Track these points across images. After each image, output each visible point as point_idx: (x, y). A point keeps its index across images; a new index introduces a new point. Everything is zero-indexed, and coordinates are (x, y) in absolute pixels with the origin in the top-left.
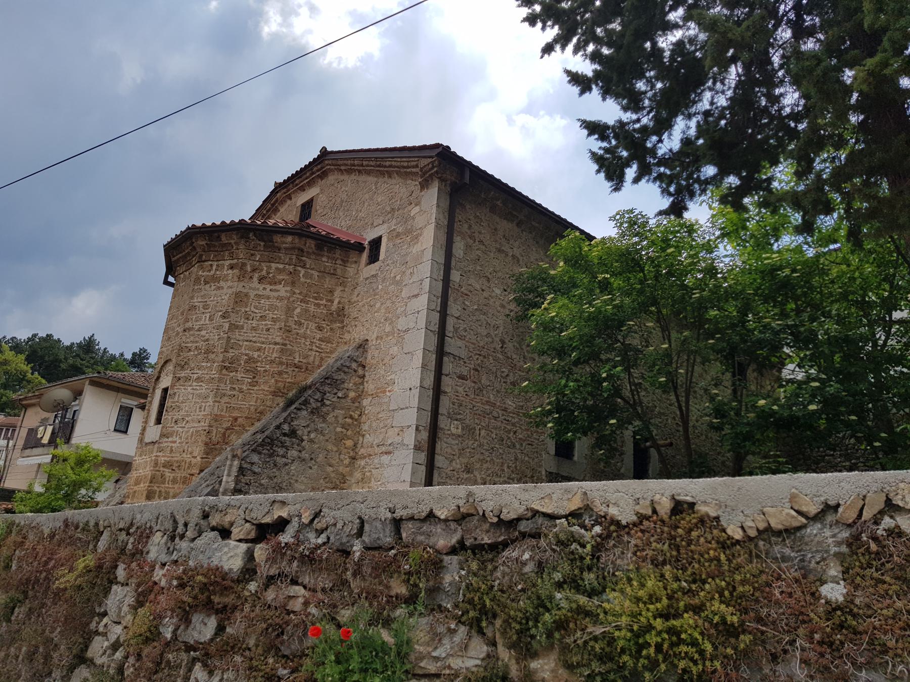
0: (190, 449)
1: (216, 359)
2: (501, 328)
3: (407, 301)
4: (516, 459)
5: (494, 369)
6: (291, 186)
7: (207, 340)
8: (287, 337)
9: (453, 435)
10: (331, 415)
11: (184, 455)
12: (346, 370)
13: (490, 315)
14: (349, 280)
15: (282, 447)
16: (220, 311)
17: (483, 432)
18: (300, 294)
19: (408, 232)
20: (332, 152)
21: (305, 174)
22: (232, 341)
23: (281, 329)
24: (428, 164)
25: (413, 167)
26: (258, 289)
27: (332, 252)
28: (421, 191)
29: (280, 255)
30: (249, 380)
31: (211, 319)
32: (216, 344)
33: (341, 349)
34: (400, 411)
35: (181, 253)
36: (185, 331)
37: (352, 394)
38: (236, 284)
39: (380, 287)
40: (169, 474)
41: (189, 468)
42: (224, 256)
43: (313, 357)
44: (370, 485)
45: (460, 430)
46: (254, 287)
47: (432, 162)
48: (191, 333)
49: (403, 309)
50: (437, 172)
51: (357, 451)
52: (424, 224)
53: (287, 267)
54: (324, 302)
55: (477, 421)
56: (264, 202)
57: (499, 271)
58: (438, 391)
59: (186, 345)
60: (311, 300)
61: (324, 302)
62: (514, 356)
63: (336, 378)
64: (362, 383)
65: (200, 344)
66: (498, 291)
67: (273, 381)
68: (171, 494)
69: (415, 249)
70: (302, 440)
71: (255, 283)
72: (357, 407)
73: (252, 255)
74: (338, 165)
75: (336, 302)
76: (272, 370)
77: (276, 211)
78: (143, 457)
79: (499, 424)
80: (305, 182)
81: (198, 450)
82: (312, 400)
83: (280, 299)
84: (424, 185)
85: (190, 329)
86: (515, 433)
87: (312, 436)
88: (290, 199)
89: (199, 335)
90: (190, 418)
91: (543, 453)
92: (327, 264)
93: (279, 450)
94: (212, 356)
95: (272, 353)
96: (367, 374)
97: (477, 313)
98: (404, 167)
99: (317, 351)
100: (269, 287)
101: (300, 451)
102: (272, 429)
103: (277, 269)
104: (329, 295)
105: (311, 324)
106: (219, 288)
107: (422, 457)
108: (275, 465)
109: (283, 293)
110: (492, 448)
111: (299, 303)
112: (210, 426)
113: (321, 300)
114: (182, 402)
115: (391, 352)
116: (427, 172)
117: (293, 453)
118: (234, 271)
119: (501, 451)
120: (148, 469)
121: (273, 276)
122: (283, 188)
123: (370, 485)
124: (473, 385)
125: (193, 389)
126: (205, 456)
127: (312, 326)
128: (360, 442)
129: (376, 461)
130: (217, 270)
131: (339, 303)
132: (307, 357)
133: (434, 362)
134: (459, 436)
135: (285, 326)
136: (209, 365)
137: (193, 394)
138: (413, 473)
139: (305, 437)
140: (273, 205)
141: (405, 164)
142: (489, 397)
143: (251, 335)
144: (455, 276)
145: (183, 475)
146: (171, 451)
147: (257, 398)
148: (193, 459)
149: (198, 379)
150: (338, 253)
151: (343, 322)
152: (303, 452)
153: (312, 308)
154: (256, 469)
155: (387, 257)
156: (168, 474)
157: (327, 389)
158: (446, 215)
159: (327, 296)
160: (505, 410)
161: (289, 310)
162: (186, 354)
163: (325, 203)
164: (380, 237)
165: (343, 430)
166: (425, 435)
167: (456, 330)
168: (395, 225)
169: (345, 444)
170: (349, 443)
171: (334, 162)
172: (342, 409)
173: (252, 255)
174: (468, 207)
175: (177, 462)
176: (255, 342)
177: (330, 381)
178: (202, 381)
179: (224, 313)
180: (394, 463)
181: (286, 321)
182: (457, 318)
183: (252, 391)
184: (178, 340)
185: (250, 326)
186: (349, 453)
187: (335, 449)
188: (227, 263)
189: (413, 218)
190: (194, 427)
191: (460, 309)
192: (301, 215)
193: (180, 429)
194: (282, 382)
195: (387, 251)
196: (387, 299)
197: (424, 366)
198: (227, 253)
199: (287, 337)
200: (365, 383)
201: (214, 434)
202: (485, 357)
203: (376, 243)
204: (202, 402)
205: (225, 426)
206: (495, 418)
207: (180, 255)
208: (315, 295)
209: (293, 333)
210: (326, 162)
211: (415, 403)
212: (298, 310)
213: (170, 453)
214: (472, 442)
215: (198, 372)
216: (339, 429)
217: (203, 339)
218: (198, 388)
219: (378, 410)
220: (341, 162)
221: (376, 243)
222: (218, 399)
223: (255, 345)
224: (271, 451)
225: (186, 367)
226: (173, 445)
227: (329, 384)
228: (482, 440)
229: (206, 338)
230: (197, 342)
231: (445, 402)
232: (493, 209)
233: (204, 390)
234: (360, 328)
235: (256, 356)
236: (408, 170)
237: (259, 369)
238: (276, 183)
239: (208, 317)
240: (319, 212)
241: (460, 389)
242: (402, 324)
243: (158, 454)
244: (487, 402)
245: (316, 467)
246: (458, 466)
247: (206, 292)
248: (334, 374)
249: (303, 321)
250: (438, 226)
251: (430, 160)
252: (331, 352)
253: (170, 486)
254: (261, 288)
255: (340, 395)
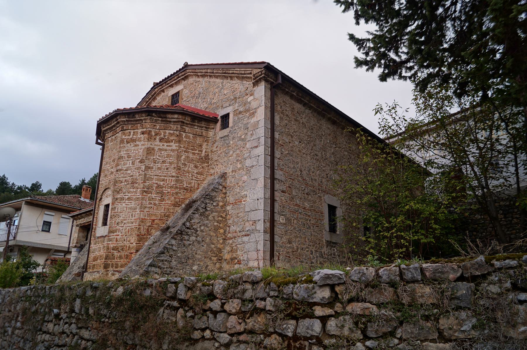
0: (128, 239)
1: (139, 186)
2: (300, 164)
3: (251, 150)
4: (311, 235)
5: (298, 186)
6: (164, 85)
7: (132, 176)
8: (179, 172)
9: (281, 223)
10: (211, 216)
11: (125, 242)
12: (217, 190)
13: (294, 157)
14: (210, 138)
15: (187, 235)
16: (138, 159)
17: (295, 221)
18: (184, 147)
19: (247, 111)
20: (192, 65)
21: (174, 77)
22: (147, 176)
23: (175, 168)
24: (258, 73)
25: (248, 74)
26: (160, 146)
27: (200, 123)
28: (253, 87)
29: (171, 125)
30: (159, 198)
31: (133, 163)
32: (138, 178)
33: (209, 179)
34: (253, 212)
35: (109, 125)
36: (117, 171)
37: (221, 204)
38: (146, 143)
39: (231, 142)
40: (117, 254)
41: (128, 249)
42: (137, 127)
43: (194, 183)
44: (237, 253)
45: (284, 221)
46: (157, 144)
47: (261, 71)
48: (122, 172)
49: (248, 155)
50: (264, 77)
51: (226, 235)
52: (258, 106)
53: (175, 132)
54: (197, 152)
55: (292, 215)
56: (147, 94)
57: (296, 132)
58: (273, 200)
59: (119, 179)
60: (190, 151)
61: (197, 152)
62: (307, 179)
63: (211, 195)
64: (225, 197)
65: (128, 178)
66: (297, 143)
67: (173, 198)
68: (119, 265)
69: (253, 120)
70: (197, 231)
71: (157, 142)
72: (224, 211)
73: (155, 126)
74: (196, 73)
75: (204, 151)
76: (172, 192)
77: (155, 99)
78: (97, 245)
79: (302, 216)
80: (174, 82)
81: (133, 239)
82: (200, 208)
83: (173, 150)
84: (256, 84)
85: (120, 170)
86: (310, 220)
87: (202, 228)
88: (164, 92)
89: (126, 173)
90: (126, 221)
91: (324, 230)
92: (197, 130)
93: (185, 237)
94: (136, 185)
95: (171, 182)
96: (227, 192)
97: (288, 156)
98: (242, 74)
99: (195, 180)
100: (166, 144)
101: (197, 237)
102: (180, 225)
103: (170, 133)
104: (200, 147)
105: (191, 164)
106: (136, 146)
107: (268, 236)
108: (184, 245)
109: (174, 147)
110: (300, 230)
111: (183, 153)
112: (139, 225)
113: (195, 150)
114: (120, 212)
115: (243, 179)
116: (258, 77)
117: (193, 238)
118: (145, 135)
119: (304, 231)
120: (102, 251)
121: (168, 138)
122: (159, 86)
123: (237, 253)
124: (289, 195)
125: (126, 205)
126: (138, 242)
127: (192, 165)
128: (228, 230)
129: (239, 240)
130: (133, 135)
131: (206, 152)
132: (190, 183)
133: (270, 184)
134: (284, 224)
135: (177, 166)
136: (135, 190)
137: (127, 207)
138: (264, 245)
139: (198, 229)
140: (153, 96)
141: (243, 72)
142: (297, 202)
143: (158, 172)
144: (277, 135)
145: (125, 254)
146: (117, 240)
147: (165, 208)
148: (131, 245)
149: (129, 199)
150: (203, 124)
151: (208, 163)
152: (198, 237)
153: (191, 156)
154: (174, 248)
155: (235, 125)
156: (116, 254)
157: (207, 201)
158: (269, 100)
159: (198, 148)
160: (304, 208)
161: (179, 157)
162: (120, 185)
163: (188, 94)
164: (228, 115)
165: (218, 224)
166: (268, 225)
167: (279, 165)
168: (237, 107)
169: (219, 232)
170: (222, 231)
171: (193, 71)
172: (216, 212)
173: (155, 126)
174: (279, 96)
175: (121, 246)
176: (161, 176)
177: (208, 197)
178: (131, 200)
179: (141, 160)
180: (251, 240)
181: (178, 163)
182: (279, 159)
183: (161, 204)
184: (113, 176)
185: (157, 167)
186: (222, 237)
187: (215, 235)
188: (140, 131)
189: (250, 103)
190: (130, 226)
191: (280, 153)
192: (172, 102)
193: (120, 228)
194: (178, 198)
195: (234, 122)
196: (237, 149)
197: (265, 186)
198: (139, 125)
199: (179, 172)
200: (227, 197)
201: (142, 230)
202: (293, 180)
203: (226, 117)
204: (133, 212)
205: (148, 225)
206: (300, 213)
207: (109, 127)
208: (192, 148)
209: (181, 170)
210: (188, 71)
211: (262, 207)
212: (183, 157)
213: (116, 242)
214: (290, 227)
215: (128, 194)
216: (216, 224)
217: (129, 175)
218: (129, 204)
219: (237, 212)
220: (199, 71)
221: (226, 117)
222: (142, 210)
223: (160, 177)
224: (182, 238)
225: (120, 192)
226: (117, 237)
227: (208, 199)
228: (295, 226)
229: (131, 175)
230: (125, 177)
231: (277, 205)
232: (292, 97)
233: (133, 205)
234: (220, 166)
235: (162, 184)
236: (245, 76)
237: (164, 191)
238: (154, 83)
239: (131, 162)
240: (184, 99)
241: (283, 198)
242: (248, 163)
243: (109, 243)
244: (296, 204)
245: (205, 245)
246: (285, 240)
247: (128, 148)
248: (210, 193)
249: (186, 163)
250: (266, 107)
251: (260, 70)
252: (203, 180)
253: (118, 260)
254: (161, 145)
255: (215, 204)
